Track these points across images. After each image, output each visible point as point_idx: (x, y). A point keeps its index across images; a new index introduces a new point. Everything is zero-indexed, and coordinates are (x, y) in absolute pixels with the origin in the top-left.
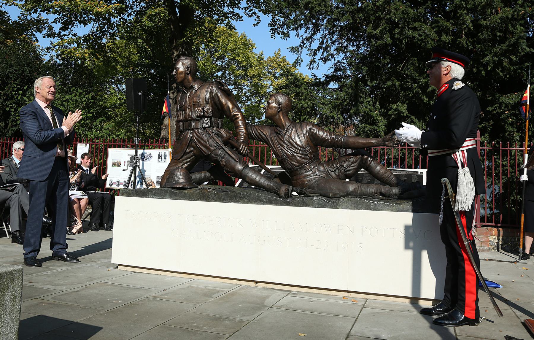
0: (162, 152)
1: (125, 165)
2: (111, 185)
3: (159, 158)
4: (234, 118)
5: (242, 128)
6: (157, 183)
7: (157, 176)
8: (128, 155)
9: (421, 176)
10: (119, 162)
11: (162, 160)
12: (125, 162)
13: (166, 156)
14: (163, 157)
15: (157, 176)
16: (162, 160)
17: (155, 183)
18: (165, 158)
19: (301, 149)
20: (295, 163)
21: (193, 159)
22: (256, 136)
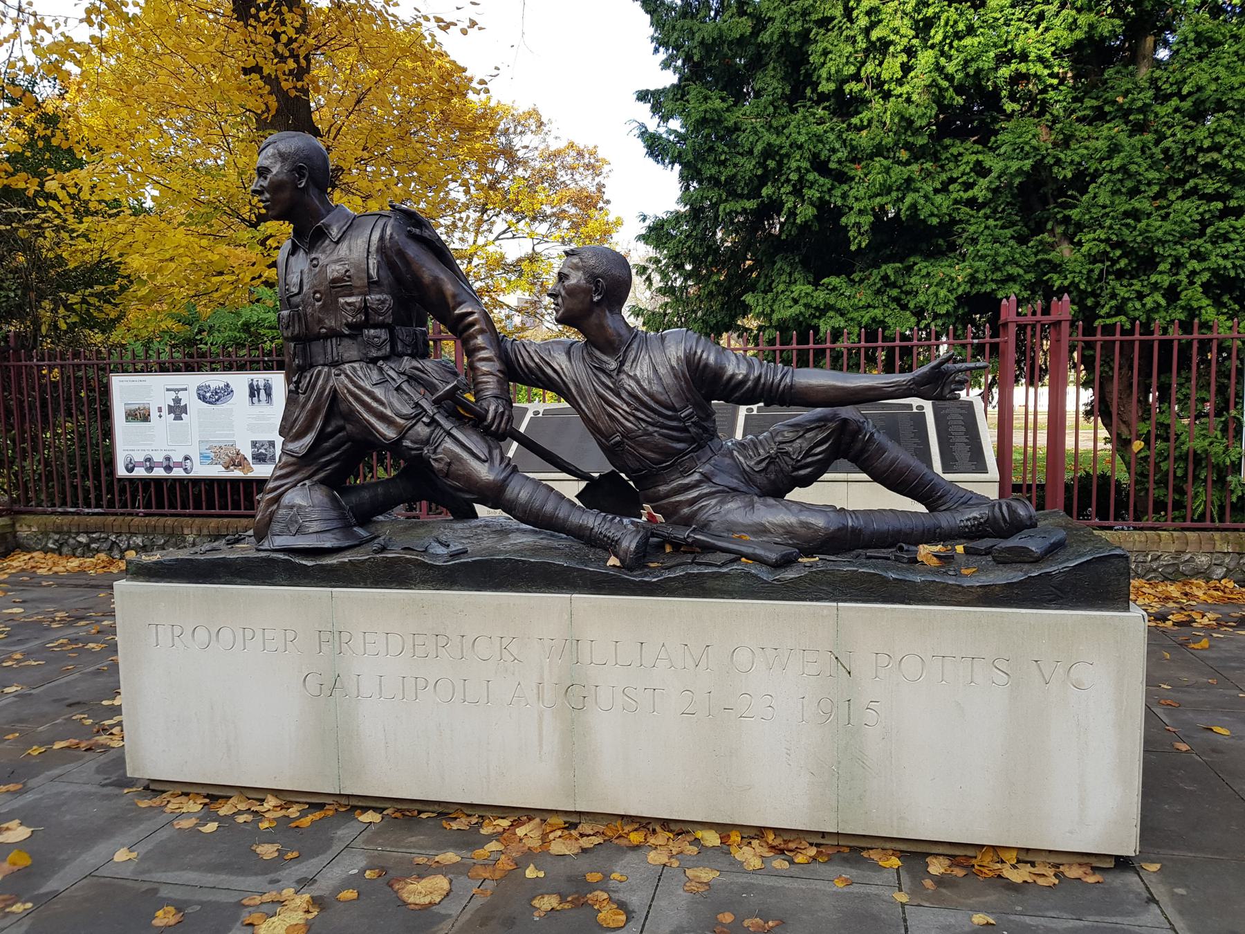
0: (260, 378)
1: (160, 416)
2: (130, 470)
3: (252, 395)
6: (253, 458)
7: (252, 442)
8: (168, 390)
9: (921, 417)
10: (144, 409)
11: (259, 401)
12: (160, 410)
13: (270, 388)
14: (262, 392)
15: (252, 442)
16: (259, 401)
17: (250, 459)
18: (269, 395)
19: (670, 413)
20: (649, 454)
21: (345, 450)
22: (646, 398)
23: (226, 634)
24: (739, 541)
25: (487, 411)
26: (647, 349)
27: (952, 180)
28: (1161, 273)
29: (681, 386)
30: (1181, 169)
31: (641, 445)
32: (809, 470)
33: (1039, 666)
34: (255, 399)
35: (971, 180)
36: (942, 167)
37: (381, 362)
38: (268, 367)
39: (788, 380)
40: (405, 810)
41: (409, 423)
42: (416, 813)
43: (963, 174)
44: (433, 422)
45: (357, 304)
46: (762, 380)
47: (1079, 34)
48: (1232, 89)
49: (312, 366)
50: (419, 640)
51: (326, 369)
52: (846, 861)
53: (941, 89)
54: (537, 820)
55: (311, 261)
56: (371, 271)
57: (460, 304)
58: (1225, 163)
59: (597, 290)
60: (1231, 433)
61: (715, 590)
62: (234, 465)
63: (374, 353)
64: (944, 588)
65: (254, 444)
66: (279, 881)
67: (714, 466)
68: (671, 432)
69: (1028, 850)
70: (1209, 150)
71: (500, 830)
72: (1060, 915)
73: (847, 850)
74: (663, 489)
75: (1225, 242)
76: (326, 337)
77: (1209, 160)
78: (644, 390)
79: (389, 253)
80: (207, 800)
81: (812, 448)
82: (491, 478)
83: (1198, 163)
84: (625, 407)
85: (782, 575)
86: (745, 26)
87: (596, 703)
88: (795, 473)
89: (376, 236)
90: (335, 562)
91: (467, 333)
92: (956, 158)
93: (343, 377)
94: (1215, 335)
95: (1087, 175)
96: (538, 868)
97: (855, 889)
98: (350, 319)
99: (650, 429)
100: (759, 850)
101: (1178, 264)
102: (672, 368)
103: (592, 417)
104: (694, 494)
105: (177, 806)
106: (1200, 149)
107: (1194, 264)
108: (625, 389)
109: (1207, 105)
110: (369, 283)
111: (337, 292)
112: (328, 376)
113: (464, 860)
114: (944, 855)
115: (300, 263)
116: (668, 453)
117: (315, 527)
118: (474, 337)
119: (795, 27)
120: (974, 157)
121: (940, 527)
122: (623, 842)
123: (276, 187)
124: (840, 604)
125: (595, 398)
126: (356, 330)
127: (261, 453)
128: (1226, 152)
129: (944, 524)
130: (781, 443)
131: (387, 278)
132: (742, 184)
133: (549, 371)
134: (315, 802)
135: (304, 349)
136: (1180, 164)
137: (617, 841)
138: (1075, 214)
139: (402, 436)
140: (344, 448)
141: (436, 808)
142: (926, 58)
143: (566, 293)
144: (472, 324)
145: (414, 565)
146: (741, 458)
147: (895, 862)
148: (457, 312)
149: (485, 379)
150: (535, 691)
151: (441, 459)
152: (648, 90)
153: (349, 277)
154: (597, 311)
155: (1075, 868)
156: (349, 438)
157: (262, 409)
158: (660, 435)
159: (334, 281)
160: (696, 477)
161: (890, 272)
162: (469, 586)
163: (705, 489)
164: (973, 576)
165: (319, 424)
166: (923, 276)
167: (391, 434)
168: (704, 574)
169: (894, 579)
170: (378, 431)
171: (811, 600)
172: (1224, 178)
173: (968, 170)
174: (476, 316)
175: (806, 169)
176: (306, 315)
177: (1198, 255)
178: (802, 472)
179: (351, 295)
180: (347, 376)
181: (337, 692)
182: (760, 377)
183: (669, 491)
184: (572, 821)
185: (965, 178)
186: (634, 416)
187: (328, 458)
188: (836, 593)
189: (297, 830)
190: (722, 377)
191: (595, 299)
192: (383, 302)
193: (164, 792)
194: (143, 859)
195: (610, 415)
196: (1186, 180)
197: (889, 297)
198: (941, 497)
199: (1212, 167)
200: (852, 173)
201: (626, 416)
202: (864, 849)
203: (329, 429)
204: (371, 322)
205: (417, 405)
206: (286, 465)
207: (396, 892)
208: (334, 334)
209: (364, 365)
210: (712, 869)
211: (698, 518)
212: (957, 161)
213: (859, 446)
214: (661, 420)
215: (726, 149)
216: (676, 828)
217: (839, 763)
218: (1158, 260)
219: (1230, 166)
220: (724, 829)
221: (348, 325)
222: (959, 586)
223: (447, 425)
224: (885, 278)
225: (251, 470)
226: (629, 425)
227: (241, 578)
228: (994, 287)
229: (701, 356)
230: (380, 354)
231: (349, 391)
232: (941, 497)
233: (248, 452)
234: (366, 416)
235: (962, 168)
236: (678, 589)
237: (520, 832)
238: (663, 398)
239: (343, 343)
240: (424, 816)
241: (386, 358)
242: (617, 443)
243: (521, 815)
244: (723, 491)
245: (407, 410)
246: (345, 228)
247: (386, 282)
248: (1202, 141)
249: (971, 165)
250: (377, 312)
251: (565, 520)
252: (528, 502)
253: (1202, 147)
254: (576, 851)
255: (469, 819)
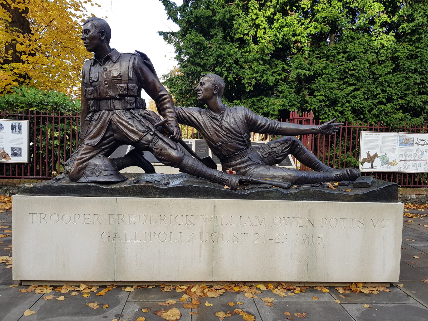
0: (16, 122)
3: (12, 129)
4: (161, 99)
5: (95, 95)
6: (11, 154)
7: (11, 148)
11: (16, 131)
14: (17, 128)
15: (11, 148)
16: (16, 131)
17: (10, 155)
18: (20, 129)
19: (239, 135)
21: (112, 144)
22: (231, 129)
23: (66, 217)
24: (266, 180)
25: (174, 131)
26: (231, 112)
27: (275, 72)
28: (338, 106)
29: (243, 126)
30: (343, 75)
31: (229, 146)
32: (282, 157)
33: (372, 221)
34: (14, 131)
35: (281, 73)
36: (271, 67)
37: (131, 110)
38: (21, 118)
39: (279, 126)
40: (142, 286)
41: (144, 134)
42: (146, 286)
43: (279, 70)
44: (154, 134)
45: (125, 87)
46: (271, 125)
47: (318, 30)
48: (358, 53)
49: (100, 110)
50: (153, 217)
51: (107, 112)
52: (311, 291)
53: (276, 42)
54: (198, 285)
55: (104, 69)
56: (130, 75)
57: (161, 91)
58: (356, 74)
59: (215, 90)
60: (356, 156)
61: (267, 197)
62: (2, 157)
63: (129, 106)
64: (343, 196)
65: (12, 149)
66: (107, 317)
67: (252, 155)
68: (239, 142)
69: (365, 283)
70: (352, 70)
71: (184, 290)
72: (387, 302)
73: (309, 288)
74: (234, 162)
75: (355, 98)
76: (108, 99)
77: (352, 73)
78: (231, 127)
79: (136, 68)
80: (52, 288)
81: (283, 150)
82: (178, 156)
83: (349, 74)
84: (223, 132)
85: (290, 191)
86: (209, 13)
87: (222, 239)
88: (277, 158)
89: (131, 63)
90: (118, 187)
91: (163, 102)
92: (276, 65)
93: (115, 115)
94: (352, 126)
95: (317, 74)
96: (209, 303)
97: (320, 300)
98: (121, 93)
99: (232, 140)
100: (281, 290)
101: (343, 104)
102: (241, 119)
103: (210, 136)
104: (246, 164)
105: (40, 291)
106: (349, 70)
107: (347, 104)
108: (224, 126)
109: (351, 57)
110: (129, 79)
111: (115, 82)
112: (108, 114)
113: (178, 302)
114: (340, 287)
115: (97, 69)
116: (238, 150)
117: (106, 173)
118: (166, 103)
119: (228, 16)
120: (282, 66)
121: (327, 177)
122: (232, 291)
123: (92, 38)
124: (311, 201)
125: (212, 129)
126: (122, 97)
127: (15, 153)
128: (357, 71)
129: (329, 176)
130: (272, 148)
131: (135, 79)
132: (208, 66)
133: (193, 119)
134: (102, 285)
135: (97, 104)
136: (343, 74)
137: (230, 291)
138: (313, 86)
139: (141, 139)
140: (111, 143)
141: (154, 284)
142: (270, 32)
143: (204, 89)
144: (165, 99)
145: (152, 188)
146: (259, 153)
147: (326, 290)
148: (160, 94)
149: (171, 119)
150: (199, 236)
151: (158, 148)
152: (162, 32)
153: (121, 76)
154: (214, 97)
155: (380, 287)
156: (115, 139)
157: (16, 135)
158: (236, 143)
159: (114, 77)
160: (246, 158)
161: (255, 100)
162: (174, 196)
163: (250, 163)
164: (349, 191)
165: (103, 133)
166: (266, 102)
167: (136, 138)
168: (264, 191)
169: (328, 193)
170: (130, 137)
171: (300, 200)
172: (355, 79)
173: (280, 69)
174: (167, 96)
175: (232, 63)
176: (100, 90)
177: (348, 102)
178: (279, 158)
179: (121, 83)
180: (117, 115)
181: (116, 240)
182: (269, 124)
183: (237, 163)
184: (210, 284)
185: (279, 72)
186: (227, 136)
187: (105, 147)
188: (309, 197)
189: (100, 296)
190: (257, 124)
191: (215, 93)
192: (134, 87)
193: (29, 286)
194: (39, 313)
195: (218, 135)
196: (344, 79)
197: (254, 108)
198: (321, 168)
199: (352, 75)
200: (244, 66)
201: (224, 135)
202: (314, 287)
203: (107, 135)
204: (129, 94)
205: (148, 127)
206: (86, 149)
207: (160, 316)
208: (113, 98)
209: (124, 111)
210: (271, 298)
211: (248, 173)
212: (276, 66)
213: (298, 150)
214: (237, 138)
215: (203, 54)
216: (250, 284)
217: (308, 257)
218: (337, 102)
219: (358, 75)
220: (265, 283)
221: (120, 95)
222: (348, 195)
223: (160, 135)
224: (253, 102)
225: (10, 159)
226: (225, 139)
227: (74, 193)
228: (289, 107)
229: (250, 116)
230: (132, 107)
231: (117, 120)
232: (321, 168)
233: (9, 152)
234: (125, 130)
235: (278, 68)
236: (254, 196)
237: (193, 290)
238: (238, 129)
239: (115, 102)
240: (150, 287)
241: (133, 109)
242: (220, 145)
243: (191, 284)
244: (255, 164)
245: (143, 129)
246: (118, 57)
247: (135, 80)
248: (350, 67)
249: (281, 68)
250: (132, 91)
251: (205, 172)
252: (192, 165)
253: (350, 69)
254: (218, 295)
255: (170, 287)
